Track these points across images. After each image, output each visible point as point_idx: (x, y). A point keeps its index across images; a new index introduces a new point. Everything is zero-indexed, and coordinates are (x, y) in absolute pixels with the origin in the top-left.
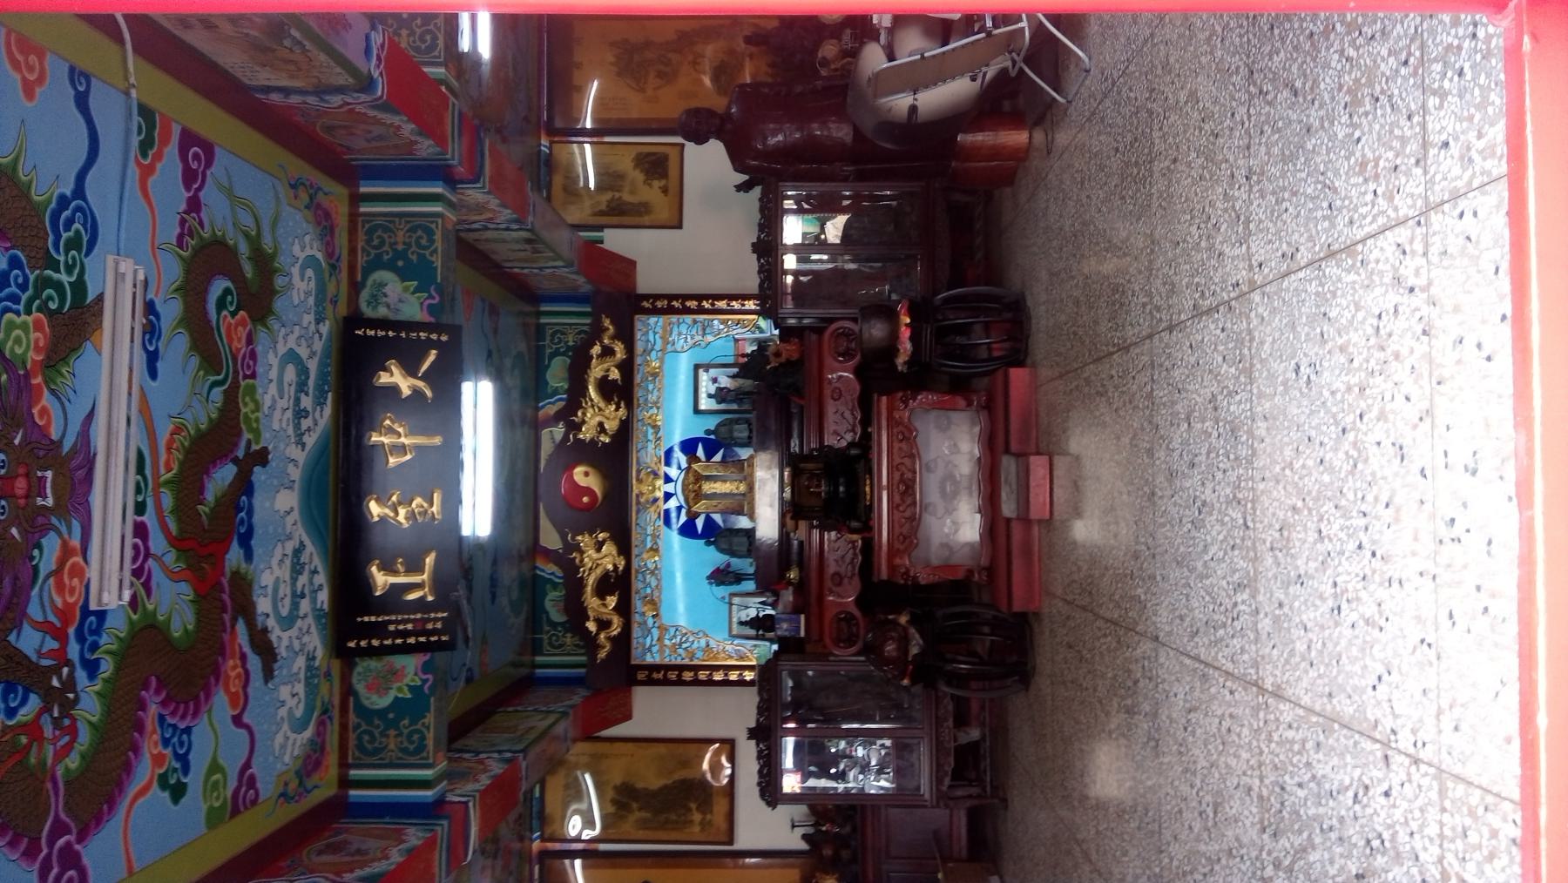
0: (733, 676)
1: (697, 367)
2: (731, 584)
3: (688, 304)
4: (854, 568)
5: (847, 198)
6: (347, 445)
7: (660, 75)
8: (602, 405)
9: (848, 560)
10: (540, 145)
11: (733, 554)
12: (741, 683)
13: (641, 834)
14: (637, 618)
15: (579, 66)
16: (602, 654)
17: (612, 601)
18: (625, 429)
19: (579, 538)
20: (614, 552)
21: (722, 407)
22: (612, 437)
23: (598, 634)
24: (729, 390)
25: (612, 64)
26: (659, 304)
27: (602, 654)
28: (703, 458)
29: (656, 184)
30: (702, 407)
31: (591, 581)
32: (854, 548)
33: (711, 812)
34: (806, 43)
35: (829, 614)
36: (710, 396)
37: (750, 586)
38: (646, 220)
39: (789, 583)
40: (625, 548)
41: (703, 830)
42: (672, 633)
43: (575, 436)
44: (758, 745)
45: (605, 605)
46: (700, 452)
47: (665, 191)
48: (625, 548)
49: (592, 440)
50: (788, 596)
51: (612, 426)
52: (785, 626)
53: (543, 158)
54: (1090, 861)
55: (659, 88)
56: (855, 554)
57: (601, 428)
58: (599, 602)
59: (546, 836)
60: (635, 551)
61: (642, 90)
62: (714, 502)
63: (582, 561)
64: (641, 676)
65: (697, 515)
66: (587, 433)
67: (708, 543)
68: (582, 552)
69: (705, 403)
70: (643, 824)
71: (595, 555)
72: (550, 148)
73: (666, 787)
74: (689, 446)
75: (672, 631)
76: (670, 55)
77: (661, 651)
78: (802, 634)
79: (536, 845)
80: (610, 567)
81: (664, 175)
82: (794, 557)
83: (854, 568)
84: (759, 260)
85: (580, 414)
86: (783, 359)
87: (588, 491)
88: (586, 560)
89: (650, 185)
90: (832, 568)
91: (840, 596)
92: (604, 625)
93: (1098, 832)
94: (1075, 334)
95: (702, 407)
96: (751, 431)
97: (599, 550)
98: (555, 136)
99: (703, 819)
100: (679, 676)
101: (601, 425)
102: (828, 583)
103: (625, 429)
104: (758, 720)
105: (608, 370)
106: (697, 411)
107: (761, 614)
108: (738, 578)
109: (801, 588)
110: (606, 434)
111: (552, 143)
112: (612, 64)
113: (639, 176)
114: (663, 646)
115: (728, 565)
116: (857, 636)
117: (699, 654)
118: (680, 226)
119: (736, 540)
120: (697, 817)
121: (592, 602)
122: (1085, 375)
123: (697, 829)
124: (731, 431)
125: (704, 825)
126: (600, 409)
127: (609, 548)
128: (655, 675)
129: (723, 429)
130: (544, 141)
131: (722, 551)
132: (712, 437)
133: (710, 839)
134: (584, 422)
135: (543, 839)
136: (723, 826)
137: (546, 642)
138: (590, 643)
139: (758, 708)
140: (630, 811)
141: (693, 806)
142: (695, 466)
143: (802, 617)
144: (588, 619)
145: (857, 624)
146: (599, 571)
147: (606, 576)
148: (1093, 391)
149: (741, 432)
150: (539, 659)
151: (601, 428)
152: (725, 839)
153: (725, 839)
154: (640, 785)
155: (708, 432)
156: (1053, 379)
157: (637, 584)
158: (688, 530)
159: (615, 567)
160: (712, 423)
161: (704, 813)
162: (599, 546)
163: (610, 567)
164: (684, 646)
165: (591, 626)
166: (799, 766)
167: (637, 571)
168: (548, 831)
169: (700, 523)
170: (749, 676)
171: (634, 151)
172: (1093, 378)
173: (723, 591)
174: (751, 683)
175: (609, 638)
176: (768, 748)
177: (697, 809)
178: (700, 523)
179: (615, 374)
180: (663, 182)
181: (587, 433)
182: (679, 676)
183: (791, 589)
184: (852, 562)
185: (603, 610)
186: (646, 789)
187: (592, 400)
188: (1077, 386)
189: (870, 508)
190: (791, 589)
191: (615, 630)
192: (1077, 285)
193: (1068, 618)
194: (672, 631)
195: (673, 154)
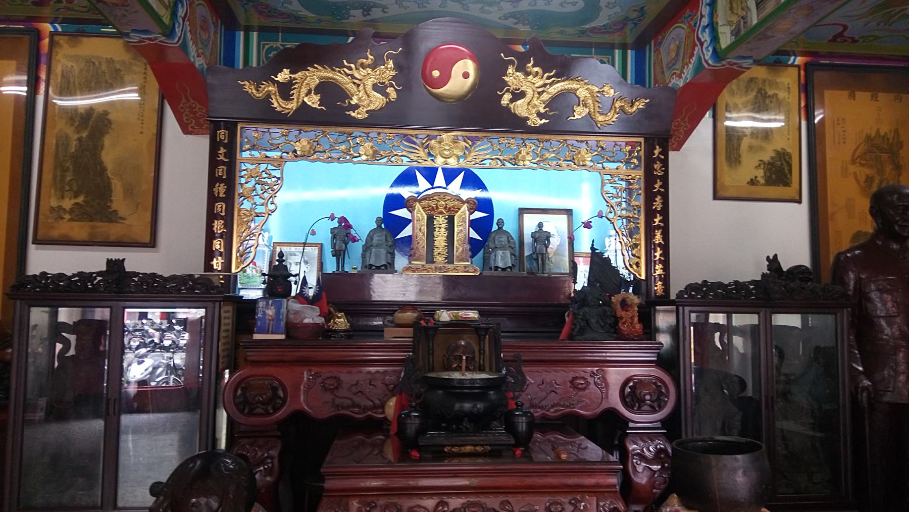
0: (218, 245)
1: (569, 212)
2: (334, 246)
3: (658, 199)
4: (348, 407)
6: (313, 362)
8: (545, 97)
9: (357, 399)
10: (796, 56)
11: (367, 248)
12: (210, 254)
13: (51, 141)
14: (294, 131)
15: (874, 98)
16: (249, 87)
17: (313, 101)
18: (518, 125)
19: (391, 64)
20: (372, 107)
21: (528, 239)
22: (507, 109)
23: (274, 82)
24: (547, 247)
25: (878, 130)
26: (657, 166)
27: (249, 87)
28: (473, 217)
29: (760, 173)
30: (527, 217)
31: (339, 77)
32: (375, 407)
33: (72, 220)
35: (283, 374)
36: (540, 225)
37: (331, 266)
38: (722, 158)
39: (328, 317)
40: (376, 120)
41: (52, 209)
42: (274, 173)
43: (511, 62)
44: (99, 274)
45: (309, 93)
46: (478, 215)
47: (753, 182)
48: (376, 120)
49: (505, 83)
50: (312, 316)
51: (520, 108)
52: (271, 312)
53: (782, 58)
55: (857, 181)
56: (365, 409)
57: (518, 95)
58: (313, 87)
59: (57, 38)
60: (373, 132)
61: (853, 161)
62: (424, 228)
63: (363, 66)
64: (222, 134)
65: (411, 209)
66: (513, 78)
67: (378, 221)
68: (373, 67)
69: (530, 223)
70: (62, 143)
71: (370, 83)
72: (792, 65)
73: (104, 170)
74: (486, 205)
75: (277, 174)
77: (253, 161)
78: (257, 337)
79: (47, 27)
80: (354, 101)
81: (769, 182)
82: (363, 322)
83: (348, 407)
84: (753, 282)
85: (536, 69)
86: (620, 313)
87: (445, 78)
88: (363, 72)
89: (757, 167)
90: (347, 376)
91: (309, 388)
92: (285, 90)
95: (527, 217)
96: (504, 269)
97: (375, 87)
98: (805, 71)
100: (220, 180)
101: (522, 95)
102: (326, 371)
103: (518, 125)
104: (136, 274)
105: (585, 105)
106: (522, 211)
107: (292, 279)
108: (339, 254)
109: (323, 333)
110: (512, 101)
111: (798, 66)
112: (878, 130)
113: (767, 156)
114: (258, 162)
115: (354, 240)
116: (251, 414)
117: (247, 205)
118: (716, 197)
119: (383, 251)
120: (67, 204)
121: (314, 76)
123: (54, 203)
124: (502, 248)
125: (58, 212)
126: (540, 93)
127: (377, 101)
128: (222, 150)
129: (504, 239)
130: (799, 60)
131: (370, 236)
132: (495, 227)
133: (41, 217)
134: (527, 74)
135: (52, 35)
136: (55, 234)
137: (272, 44)
138: (267, 72)
139: (154, 275)
140: (78, 130)
141: (80, 199)
142: (465, 207)
143: (282, 337)
144: (293, 72)
145: (268, 414)
146: (351, 88)
147: (344, 95)
149: (503, 258)
150: (255, 35)
151: (518, 95)
152: (39, 237)
153: (39, 237)
154: (107, 141)
155: (500, 222)
157: (333, 134)
158: (393, 201)
159: (357, 107)
160: (510, 227)
161: (71, 211)
162: (380, 88)
163: (354, 101)
164: (258, 187)
165: (283, 76)
167: (350, 134)
168: (62, 40)
169: (403, 213)
170: (217, 263)
171: (792, 150)
173: (324, 235)
174: (208, 267)
175: (268, 95)
176: (95, 288)
177: (76, 204)
178: (403, 213)
179: (580, 113)
180: (762, 181)
181: (513, 78)
182: (220, 180)
183: (321, 320)
184: (355, 405)
185: (304, 90)
186: (102, 147)
187: (551, 84)
189: (439, 455)
190: (321, 320)
191: (277, 103)
194: (277, 174)
195: (790, 192)
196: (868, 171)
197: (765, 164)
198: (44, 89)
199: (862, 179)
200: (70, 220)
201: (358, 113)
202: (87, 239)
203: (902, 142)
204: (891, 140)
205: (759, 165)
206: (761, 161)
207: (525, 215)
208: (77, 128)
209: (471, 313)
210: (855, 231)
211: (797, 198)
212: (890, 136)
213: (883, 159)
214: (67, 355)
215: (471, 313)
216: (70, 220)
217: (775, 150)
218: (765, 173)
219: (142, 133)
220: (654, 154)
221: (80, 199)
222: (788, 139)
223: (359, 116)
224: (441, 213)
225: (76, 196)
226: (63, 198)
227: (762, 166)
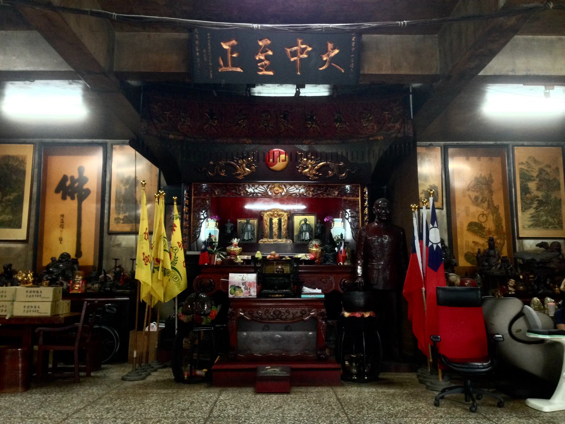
5: (531, 278)
7: (476, 198)
15: (479, 159)
33: (123, 223)
34: (494, 268)
54: (74, 414)
55: (470, 197)
76: (486, 203)
93: (88, 418)
94: (363, 408)
99: (120, 219)
100: (186, 228)
122: (341, 414)
148: (332, 419)
156: (336, 395)
159: (240, 174)
161: (123, 220)
163: (239, 172)
166: (22, 161)
172: (340, 419)
177: (125, 216)
182: (186, 228)
188: (334, 409)
192: (390, 409)
193: (207, 403)
196: (476, 194)
197: (425, 192)
198: (309, 367)
199: (473, 197)
200: (122, 223)
201: (240, 177)
202: (130, 231)
203: (492, 180)
204: (487, 179)
205: (423, 192)
206: (423, 190)
207: (295, 216)
208: (124, 184)
209: (158, 218)
210: (470, 222)
211: (441, 207)
212: (487, 177)
213: (483, 188)
214: (258, 73)
215: (158, 218)
216: (122, 223)
217: (429, 185)
218: (425, 196)
219: (151, 185)
220: (206, 214)
221: (557, 286)
222: (436, 180)
223: (240, 178)
224: (276, 217)
225: (125, 213)
226: (119, 214)
227: (424, 193)
